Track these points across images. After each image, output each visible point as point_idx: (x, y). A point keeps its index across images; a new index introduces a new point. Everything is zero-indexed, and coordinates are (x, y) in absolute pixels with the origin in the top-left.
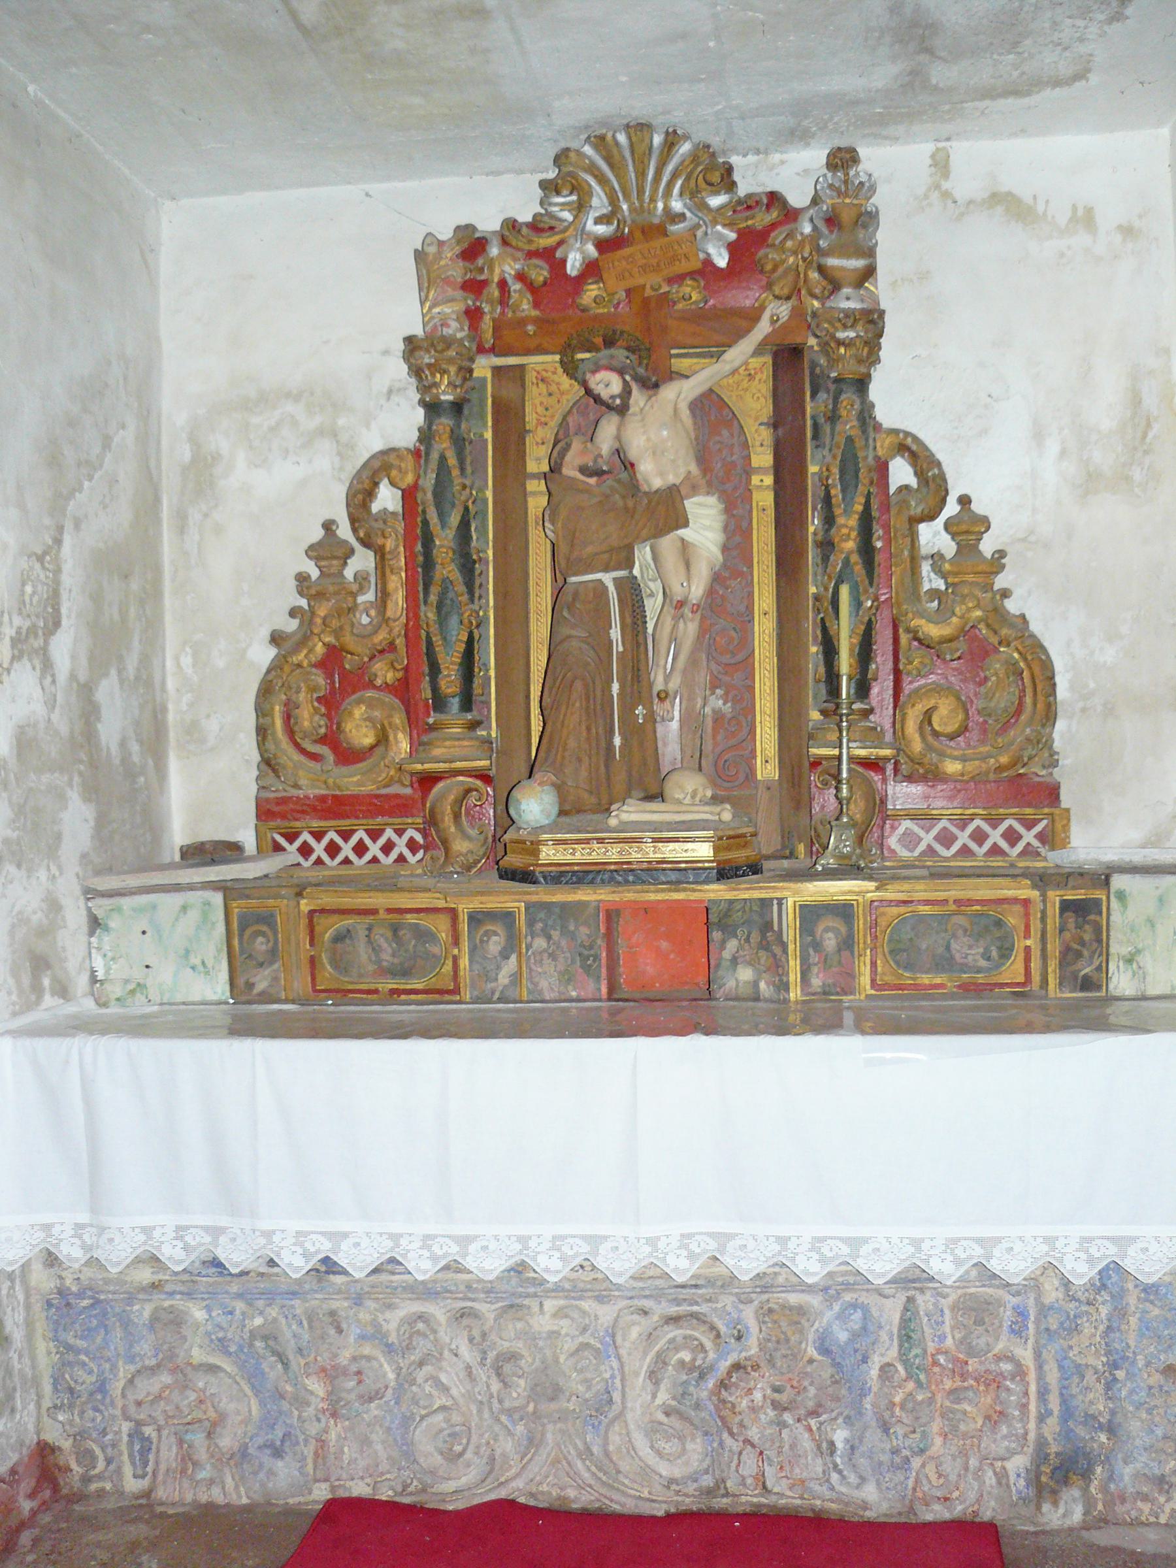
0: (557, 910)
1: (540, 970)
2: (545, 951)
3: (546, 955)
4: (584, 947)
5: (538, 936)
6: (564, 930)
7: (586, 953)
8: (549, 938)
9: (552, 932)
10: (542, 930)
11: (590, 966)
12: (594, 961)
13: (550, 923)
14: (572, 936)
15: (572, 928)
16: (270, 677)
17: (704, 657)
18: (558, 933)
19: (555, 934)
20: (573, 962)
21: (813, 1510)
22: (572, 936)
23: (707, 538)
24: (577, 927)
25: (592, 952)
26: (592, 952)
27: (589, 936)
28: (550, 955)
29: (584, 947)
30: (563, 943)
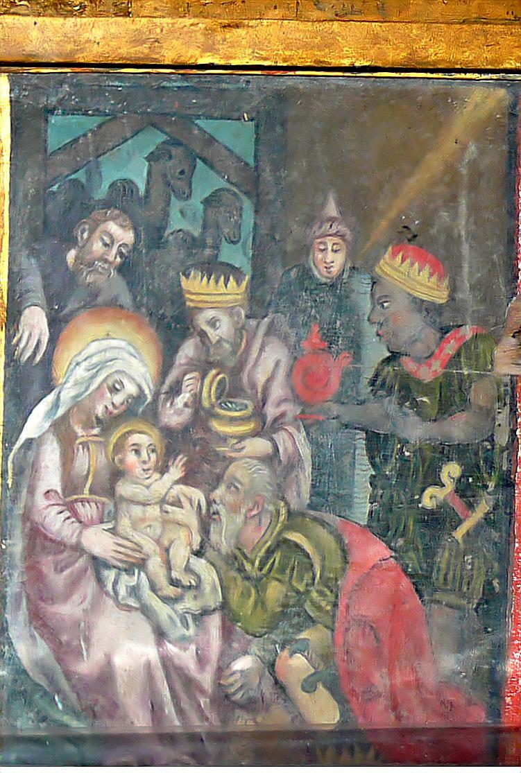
0: (236, 136)
1: (99, 541)
2: (139, 410)
3: (144, 438)
4: (406, 390)
5: (97, 304)
6: (280, 286)
7: (416, 431)
8: (172, 325)
9: (196, 286)
10: (126, 268)
11: (438, 521)
12: (466, 491)
13: (182, 219)
14: (328, 315)
15: (330, 259)
16: (207, 637)
17: (17, 575)
18: (233, 291)
19: (216, 301)
20: (329, 493)
21: (47, 439)
22: (328, 315)
23: (95, 436)
24: (361, 261)
25: (458, 428)
26: (458, 428)
27: (444, 320)
28: (174, 443)
29: (406, 390)
30: (269, 363)
